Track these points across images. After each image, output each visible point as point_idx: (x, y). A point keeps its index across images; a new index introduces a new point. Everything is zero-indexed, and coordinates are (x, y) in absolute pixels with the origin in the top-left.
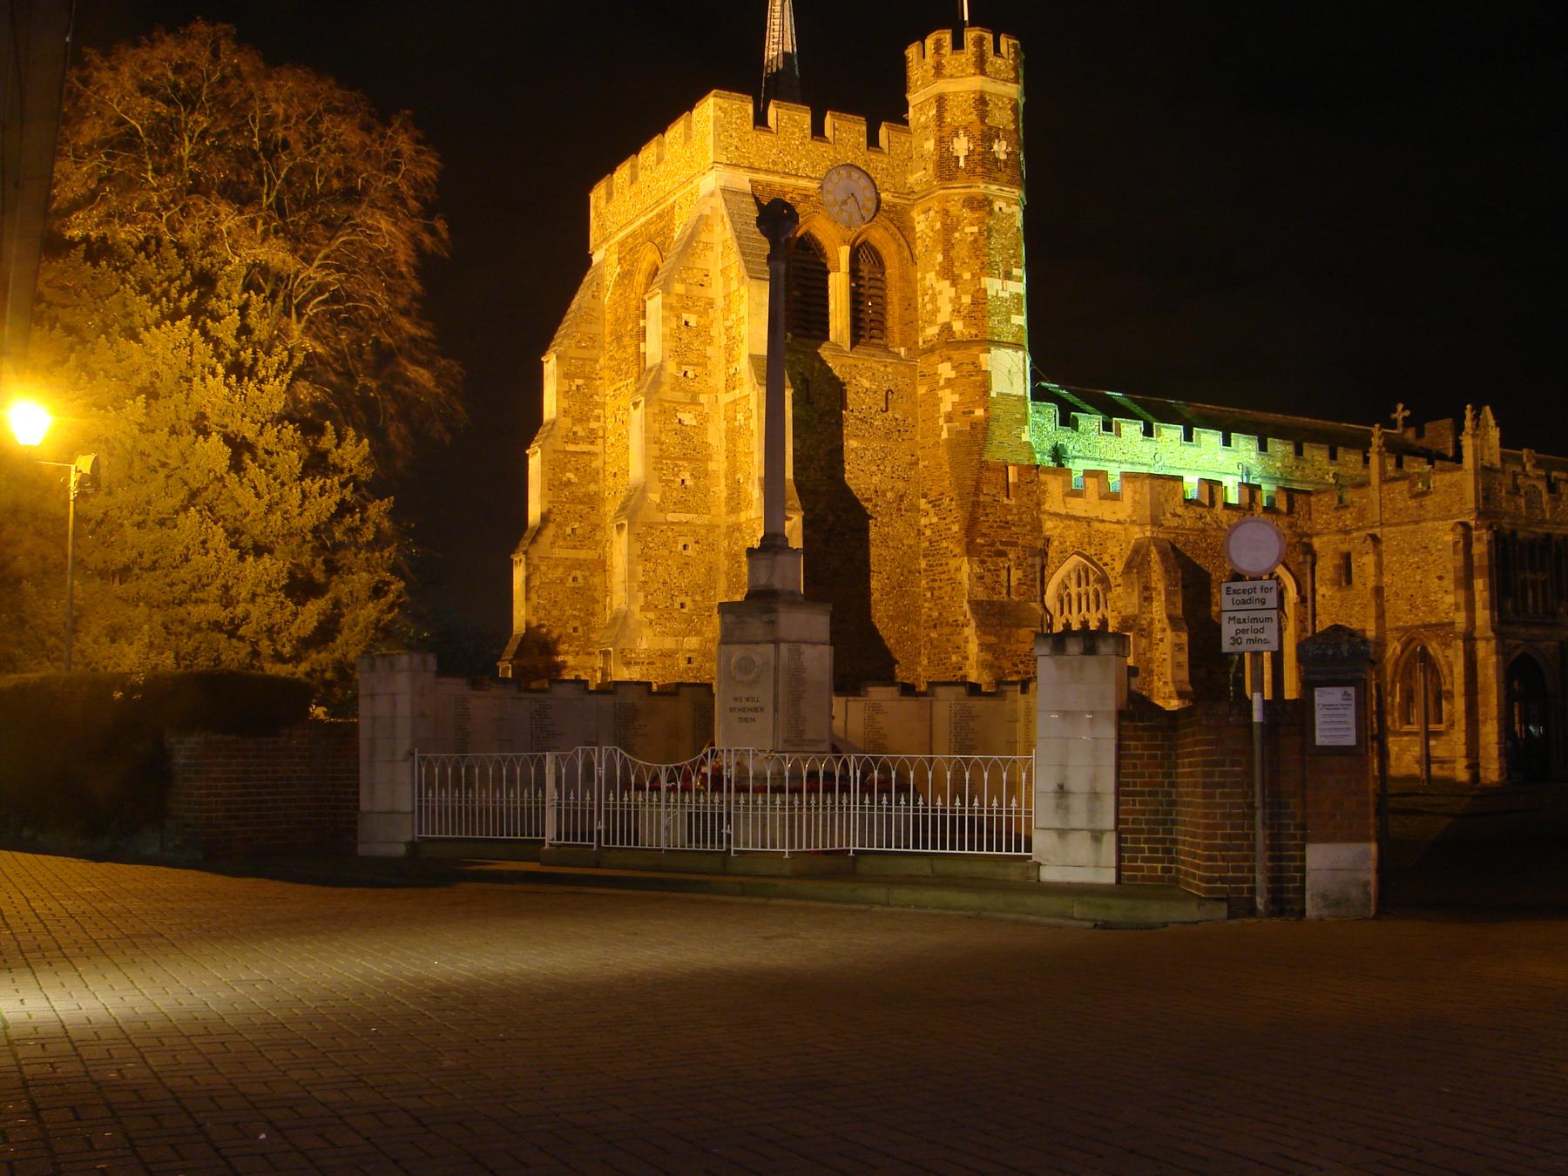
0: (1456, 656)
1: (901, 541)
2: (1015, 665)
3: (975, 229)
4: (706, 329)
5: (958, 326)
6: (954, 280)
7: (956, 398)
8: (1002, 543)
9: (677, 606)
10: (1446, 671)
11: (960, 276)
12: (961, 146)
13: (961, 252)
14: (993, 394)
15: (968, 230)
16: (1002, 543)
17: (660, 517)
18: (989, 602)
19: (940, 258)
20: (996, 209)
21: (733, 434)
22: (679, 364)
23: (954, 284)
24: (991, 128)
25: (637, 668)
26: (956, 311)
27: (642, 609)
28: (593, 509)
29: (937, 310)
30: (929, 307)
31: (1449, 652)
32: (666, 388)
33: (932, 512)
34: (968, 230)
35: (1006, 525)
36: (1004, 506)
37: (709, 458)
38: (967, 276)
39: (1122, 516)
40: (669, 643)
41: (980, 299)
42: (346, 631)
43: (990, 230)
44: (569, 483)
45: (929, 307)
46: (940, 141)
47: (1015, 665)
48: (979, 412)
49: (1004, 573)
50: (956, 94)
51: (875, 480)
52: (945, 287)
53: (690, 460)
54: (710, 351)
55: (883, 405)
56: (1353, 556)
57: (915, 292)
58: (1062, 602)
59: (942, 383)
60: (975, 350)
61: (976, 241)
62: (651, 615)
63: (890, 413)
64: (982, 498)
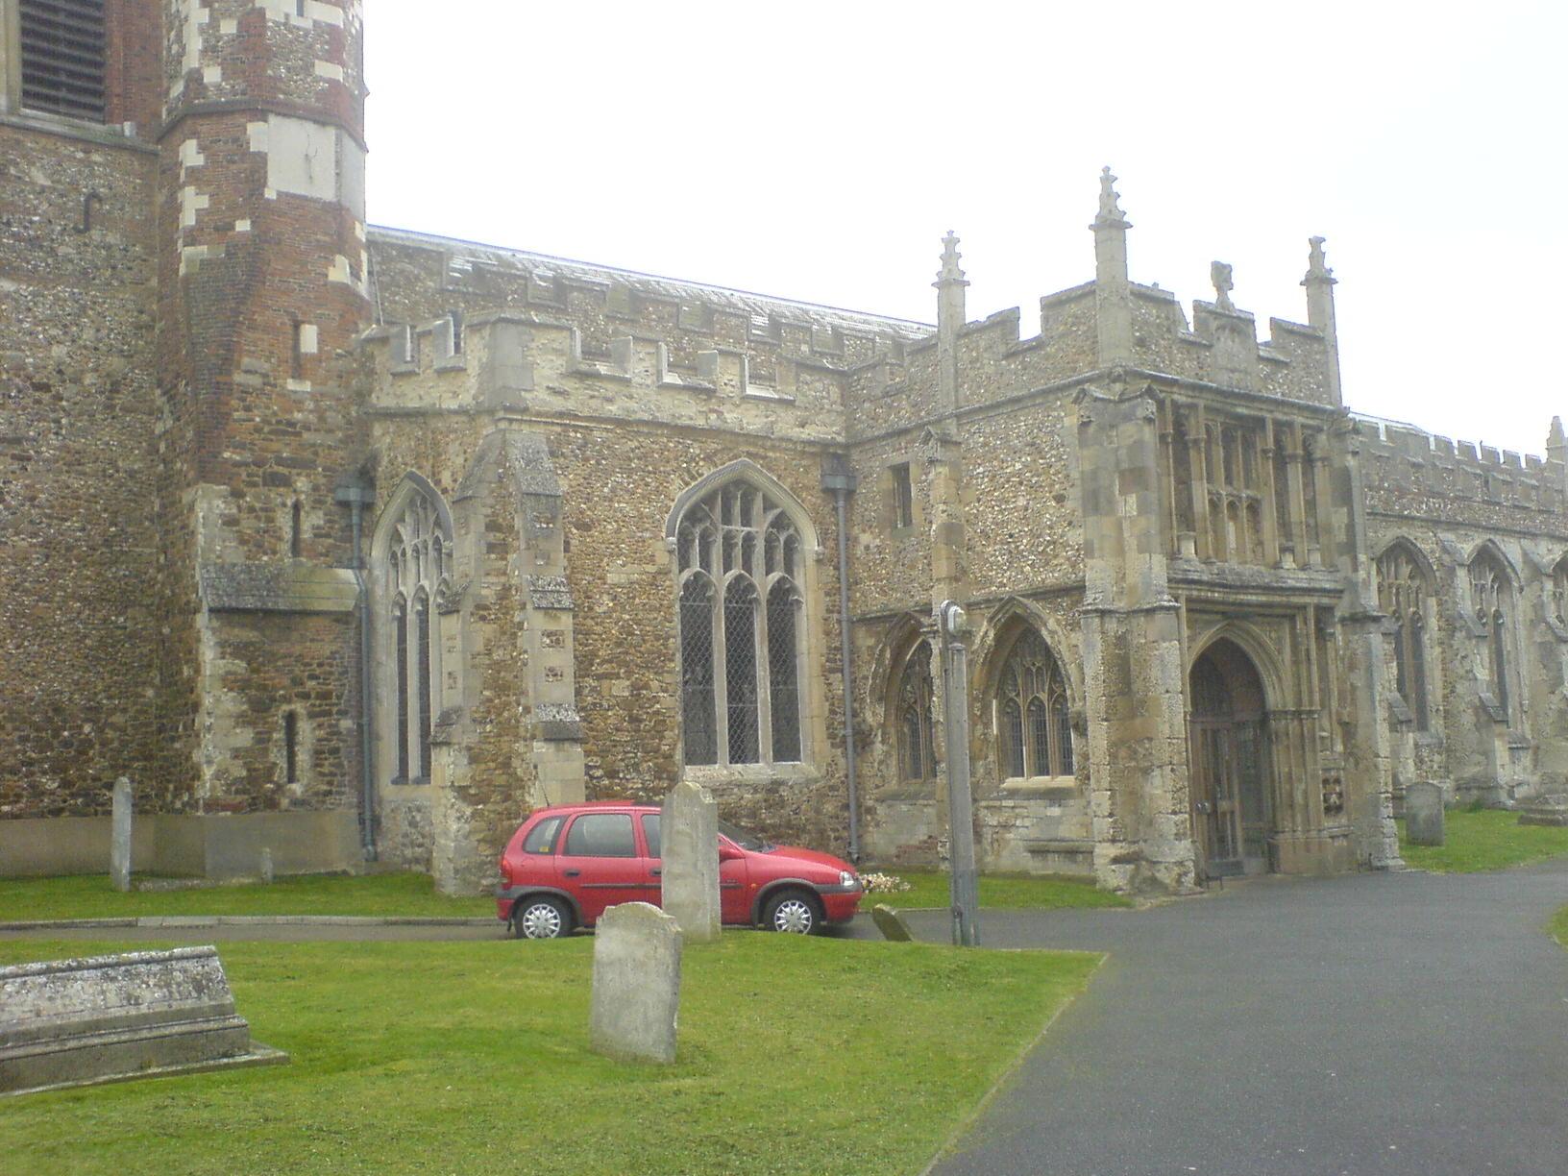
0: (1089, 644)
1: (113, 463)
2: (297, 682)
5: (212, 75)
7: (204, 202)
8: (280, 461)
10: (1072, 670)
14: (270, 194)
16: (280, 461)
21: (1124, 671)
26: (210, 51)
28: (1150, 739)
30: (175, 48)
31: (1076, 638)
36: (284, 395)
48: (243, 226)
49: (284, 521)
51: (57, 351)
55: (76, 217)
56: (913, 471)
57: (157, 27)
63: (96, 234)
64: (238, 377)
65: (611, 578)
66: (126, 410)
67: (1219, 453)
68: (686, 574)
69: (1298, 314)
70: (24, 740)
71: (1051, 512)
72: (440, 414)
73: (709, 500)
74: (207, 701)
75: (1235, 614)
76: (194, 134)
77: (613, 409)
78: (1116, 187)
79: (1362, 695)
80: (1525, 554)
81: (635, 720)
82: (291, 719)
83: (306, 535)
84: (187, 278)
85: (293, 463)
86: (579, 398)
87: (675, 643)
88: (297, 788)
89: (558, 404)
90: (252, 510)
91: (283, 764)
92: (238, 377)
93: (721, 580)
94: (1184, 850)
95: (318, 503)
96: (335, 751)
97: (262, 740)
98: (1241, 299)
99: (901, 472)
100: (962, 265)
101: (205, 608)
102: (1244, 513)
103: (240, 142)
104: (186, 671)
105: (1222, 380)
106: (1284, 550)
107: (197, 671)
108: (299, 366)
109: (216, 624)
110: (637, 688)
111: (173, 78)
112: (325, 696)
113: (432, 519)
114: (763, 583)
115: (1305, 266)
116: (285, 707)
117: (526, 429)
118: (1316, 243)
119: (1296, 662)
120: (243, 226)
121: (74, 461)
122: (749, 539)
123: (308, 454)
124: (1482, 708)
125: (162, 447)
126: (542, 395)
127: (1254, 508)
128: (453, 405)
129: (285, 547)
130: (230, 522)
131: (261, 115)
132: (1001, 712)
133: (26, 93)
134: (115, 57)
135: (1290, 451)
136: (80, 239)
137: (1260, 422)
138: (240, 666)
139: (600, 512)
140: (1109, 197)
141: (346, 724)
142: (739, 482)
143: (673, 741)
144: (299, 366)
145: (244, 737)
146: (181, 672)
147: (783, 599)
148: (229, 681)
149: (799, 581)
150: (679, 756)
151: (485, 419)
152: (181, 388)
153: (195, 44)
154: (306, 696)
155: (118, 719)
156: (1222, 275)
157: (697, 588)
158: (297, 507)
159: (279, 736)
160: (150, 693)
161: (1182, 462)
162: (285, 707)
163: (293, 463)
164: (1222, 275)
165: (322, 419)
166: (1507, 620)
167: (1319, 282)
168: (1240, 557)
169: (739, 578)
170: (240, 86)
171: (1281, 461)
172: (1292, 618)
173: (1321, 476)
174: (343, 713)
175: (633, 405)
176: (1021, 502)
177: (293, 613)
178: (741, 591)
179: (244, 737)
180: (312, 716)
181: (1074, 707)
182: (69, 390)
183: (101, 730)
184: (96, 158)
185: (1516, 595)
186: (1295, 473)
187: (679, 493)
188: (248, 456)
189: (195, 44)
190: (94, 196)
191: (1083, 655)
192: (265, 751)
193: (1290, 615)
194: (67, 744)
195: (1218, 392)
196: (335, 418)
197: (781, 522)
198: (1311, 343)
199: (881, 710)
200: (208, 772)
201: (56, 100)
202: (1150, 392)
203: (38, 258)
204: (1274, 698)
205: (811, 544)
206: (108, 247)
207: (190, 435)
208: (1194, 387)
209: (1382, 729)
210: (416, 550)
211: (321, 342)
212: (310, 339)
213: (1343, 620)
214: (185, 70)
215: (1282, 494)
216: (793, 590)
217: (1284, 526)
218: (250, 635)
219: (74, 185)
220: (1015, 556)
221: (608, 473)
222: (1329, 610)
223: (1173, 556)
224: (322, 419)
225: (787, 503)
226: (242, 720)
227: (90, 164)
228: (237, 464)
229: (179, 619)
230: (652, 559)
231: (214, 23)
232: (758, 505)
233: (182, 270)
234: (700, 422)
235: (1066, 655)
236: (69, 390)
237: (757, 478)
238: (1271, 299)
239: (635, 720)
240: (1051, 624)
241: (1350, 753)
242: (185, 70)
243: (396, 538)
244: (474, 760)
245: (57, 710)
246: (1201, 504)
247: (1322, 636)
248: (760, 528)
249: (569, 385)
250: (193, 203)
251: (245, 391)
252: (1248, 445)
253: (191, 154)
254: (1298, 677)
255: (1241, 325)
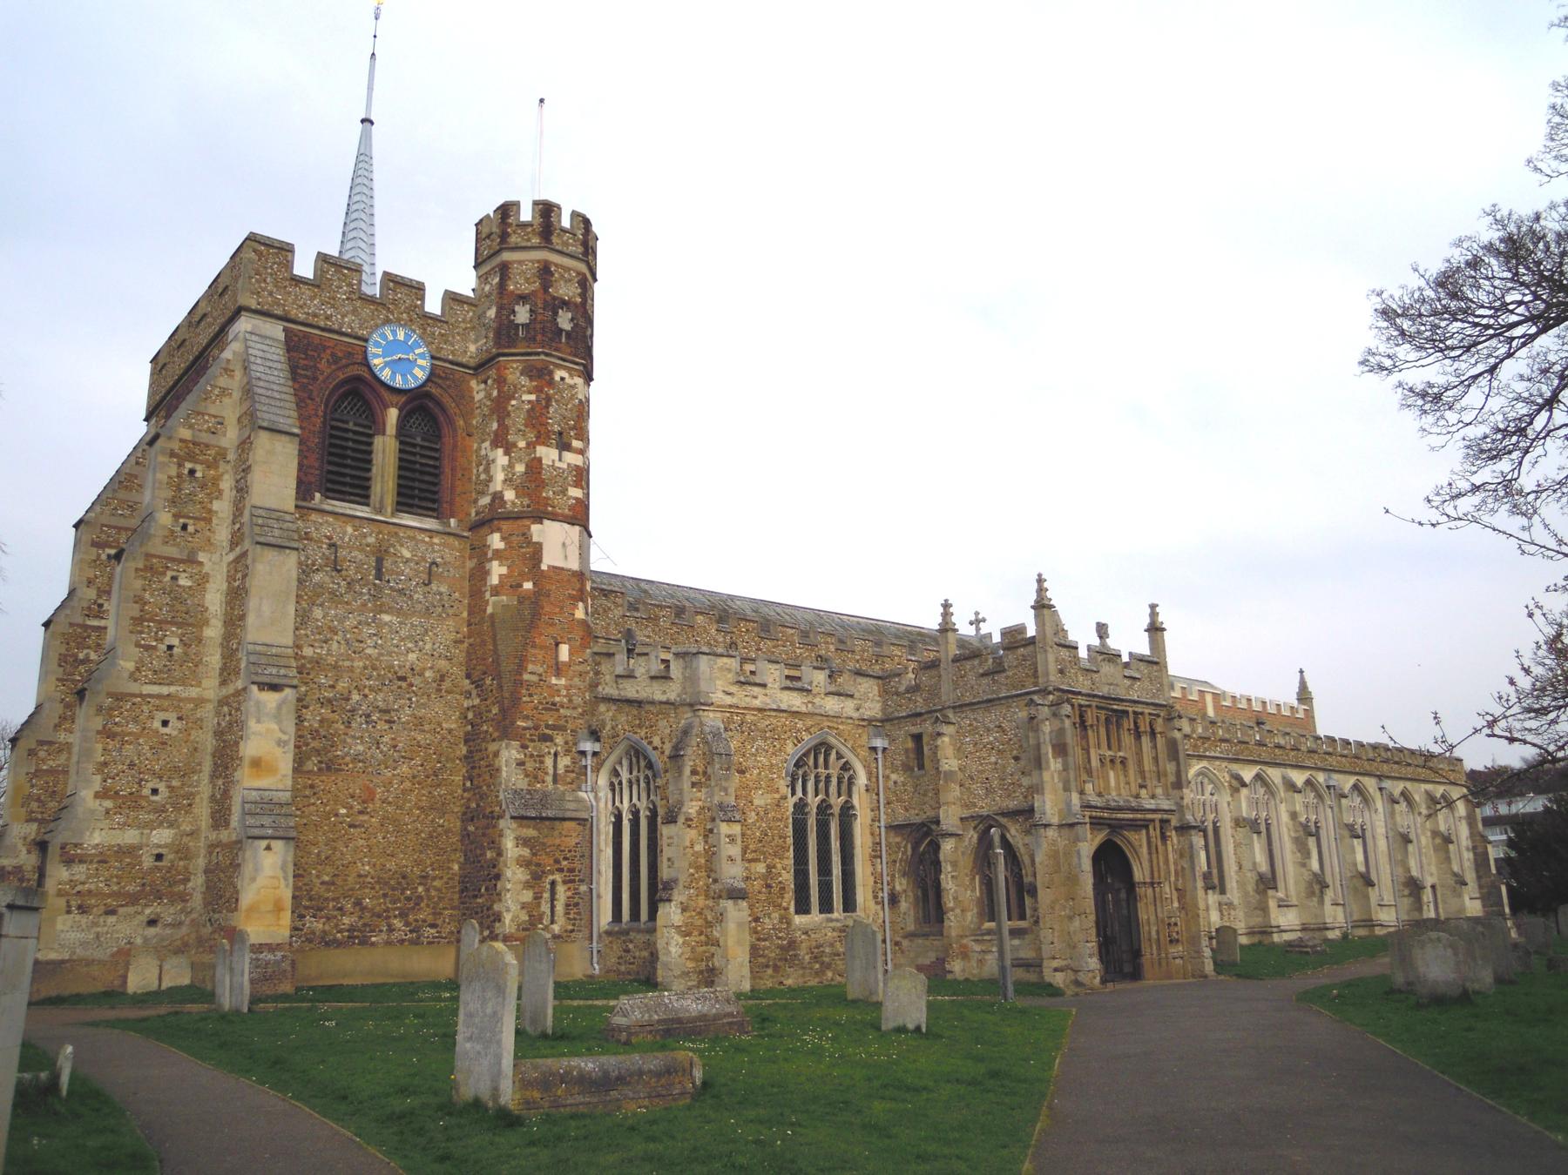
1: (440, 724)
3: (533, 397)
4: (216, 480)
5: (509, 495)
6: (509, 449)
7: (504, 570)
8: (547, 727)
9: (146, 792)
10: (1026, 859)
11: (514, 445)
12: (522, 315)
13: (518, 420)
14: (544, 567)
15: (526, 397)
16: (547, 727)
17: (134, 688)
18: (529, 792)
19: (495, 426)
20: (557, 378)
22: (176, 516)
23: (507, 453)
24: (554, 298)
25: (82, 868)
27: (97, 795)
29: (490, 479)
30: (483, 477)
32: (158, 541)
33: (474, 693)
34: (526, 397)
35: (553, 707)
36: (551, 686)
37: (206, 622)
38: (522, 444)
39: (672, 696)
40: (130, 837)
41: (535, 466)
42: (665, 849)
43: (549, 399)
44: (87, 660)
45: (483, 477)
46: (500, 309)
47: (557, 861)
48: (528, 585)
49: (549, 762)
50: (520, 262)
51: (412, 657)
52: (501, 458)
53: (179, 625)
54: (216, 505)
55: (425, 576)
56: (925, 739)
58: (613, 790)
59: (490, 555)
60: (527, 522)
61: (532, 409)
62: (108, 804)
63: (434, 586)
64: (526, 677)
65: (756, 802)
66: (448, 692)
67: (1103, 731)
68: (795, 799)
69: (1143, 648)
70: (385, 895)
71: (1012, 766)
72: (652, 703)
73: (806, 754)
74: (509, 873)
75: (1116, 827)
76: (499, 530)
77: (757, 703)
78: (1046, 585)
79: (1188, 872)
80: (1284, 778)
81: (769, 886)
82: (553, 883)
83: (561, 771)
84: (492, 615)
85: (554, 728)
86: (741, 697)
87: (790, 841)
88: (556, 928)
89: (728, 700)
90: (532, 756)
91: (548, 912)
92: (526, 677)
93: (813, 801)
94: (1094, 963)
95: (568, 752)
96: (577, 904)
97: (538, 897)
98: (1113, 643)
99: (918, 738)
100: (954, 619)
101: (507, 816)
102: (1119, 766)
103: (526, 536)
104: (489, 854)
105: (1104, 690)
106: (1141, 786)
107: (500, 854)
108: (558, 670)
109: (514, 825)
110: (769, 867)
111: (483, 493)
112: (571, 870)
113: (643, 764)
114: (837, 802)
115: (1148, 620)
116: (551, 877)
117: (711, 715)
118: (1153, 607)
119: (1150, 853)
120: (528, 585)
121: (419, 723)
122: (828, 777)
123: (562, 722)
124: (1261, 877)
125: (470, 715)
126: (720, 695)
127: (1123, 762)
128: (664, 698)
129: (549, 779)
130: (521, 764)
131: (539, 519)
132: (981, 883)
133: (398, 503)
134: (446, 479)
135: (1142, 729)
136: (427, 589)
137: (1127, 712)
138: (526, 852)
139: (750, 763)
140: (1041, 590)
141: (583, 888)
142: (822, 744)
143: (789, 900)
144: (558, 670)
145: (528, 896)
146: (484, 854)
147: (847, 813)
148: (524, 863)
149: (855, 801)
150: (792, 909)
151: (687, 708)
152: (488, 682)
153: (500, 476)
154: (561, 870)
155: (437, 883)
156: (1102, 630)
157: (801, 807)
158: (556, 755)
159: (546, 895)
160: (456, 867)
161: (1085, 737)
162: (551, 877)
163: (554, 728)
164: (1102, 630)
165: (570, 701)
166: (1273, 822)
167: (1155, 629)
168: (1116, 788)
169: (823, 801)
170: (526, 501)
171: (1138, 736)
172: (1147, 827)
173: (1160, 740)
174: (581, 881)
175: (768, 700)
176: (993, 759)
177: (556, 819)
178: (824, 808)
179: (528, 896)
180: (565, 882)
181: (1027, 880)
182: (417, 681)
183: (427, 890)
184: (436, 540)
185: (1422, 283)
186: (1145, 740)
187: (792, 750)
188: (530, 724)
189: (500, 476)
190: (434, 563)
191: (1042, 850)
192: (539, 905)
193: (1145, 825)
194: (409, 899)
195: (1103, 697)
196: (577, 700)
197: (846, 767)
198: (1154, 662)
199: (904, 881)
200: (507, 918)
201: (411, 506)
202: (1068, 701)
203: (402, 603)
204: (1138, 875)
205: (862, 779)
206: (441, 594)
207: (495, 710)
208: (1089, 695)
209: (1200, 893)
210: (630, 782)
211: (571, 654)
212: (564, 652)
213: (1176, 828)
214: (491, 490)
215: (1139, 753)
216: (853, 807)
217: (1142, 773)
218: (530, 832)
219: (423, 559)
220: (989, 791)
221: (754, 740)
222: (1168, 821)
223: (1082, 792)
224: (570, 701)
225: (849, 756)
226: (527, 885)
227: (432, 544)
228: (525, 729)
229: (485, 822)
230: (777, 791)
231: (511, 466)
232: (833, 756)
233: (489, 610)
234: (804, 709)
235: (1022, 850)
236: (417, 681)
237: (833, 741)
238: (1130, 641)
239: (769, 886)
240: (1013, 831)
241: (1182, 908)
242: (491, 490)
243: (616, 773)
244: (684, 910)
245: (404, 877)
246: (1095, 763)
247: (1164, 838)
248: (834, 772)
249: (734, 689)
250: (497, 571)
251: (529, 685)
252: (1119, 726)
253: (496, 541)
254: (1151, 861)
255: (1114, 657)
